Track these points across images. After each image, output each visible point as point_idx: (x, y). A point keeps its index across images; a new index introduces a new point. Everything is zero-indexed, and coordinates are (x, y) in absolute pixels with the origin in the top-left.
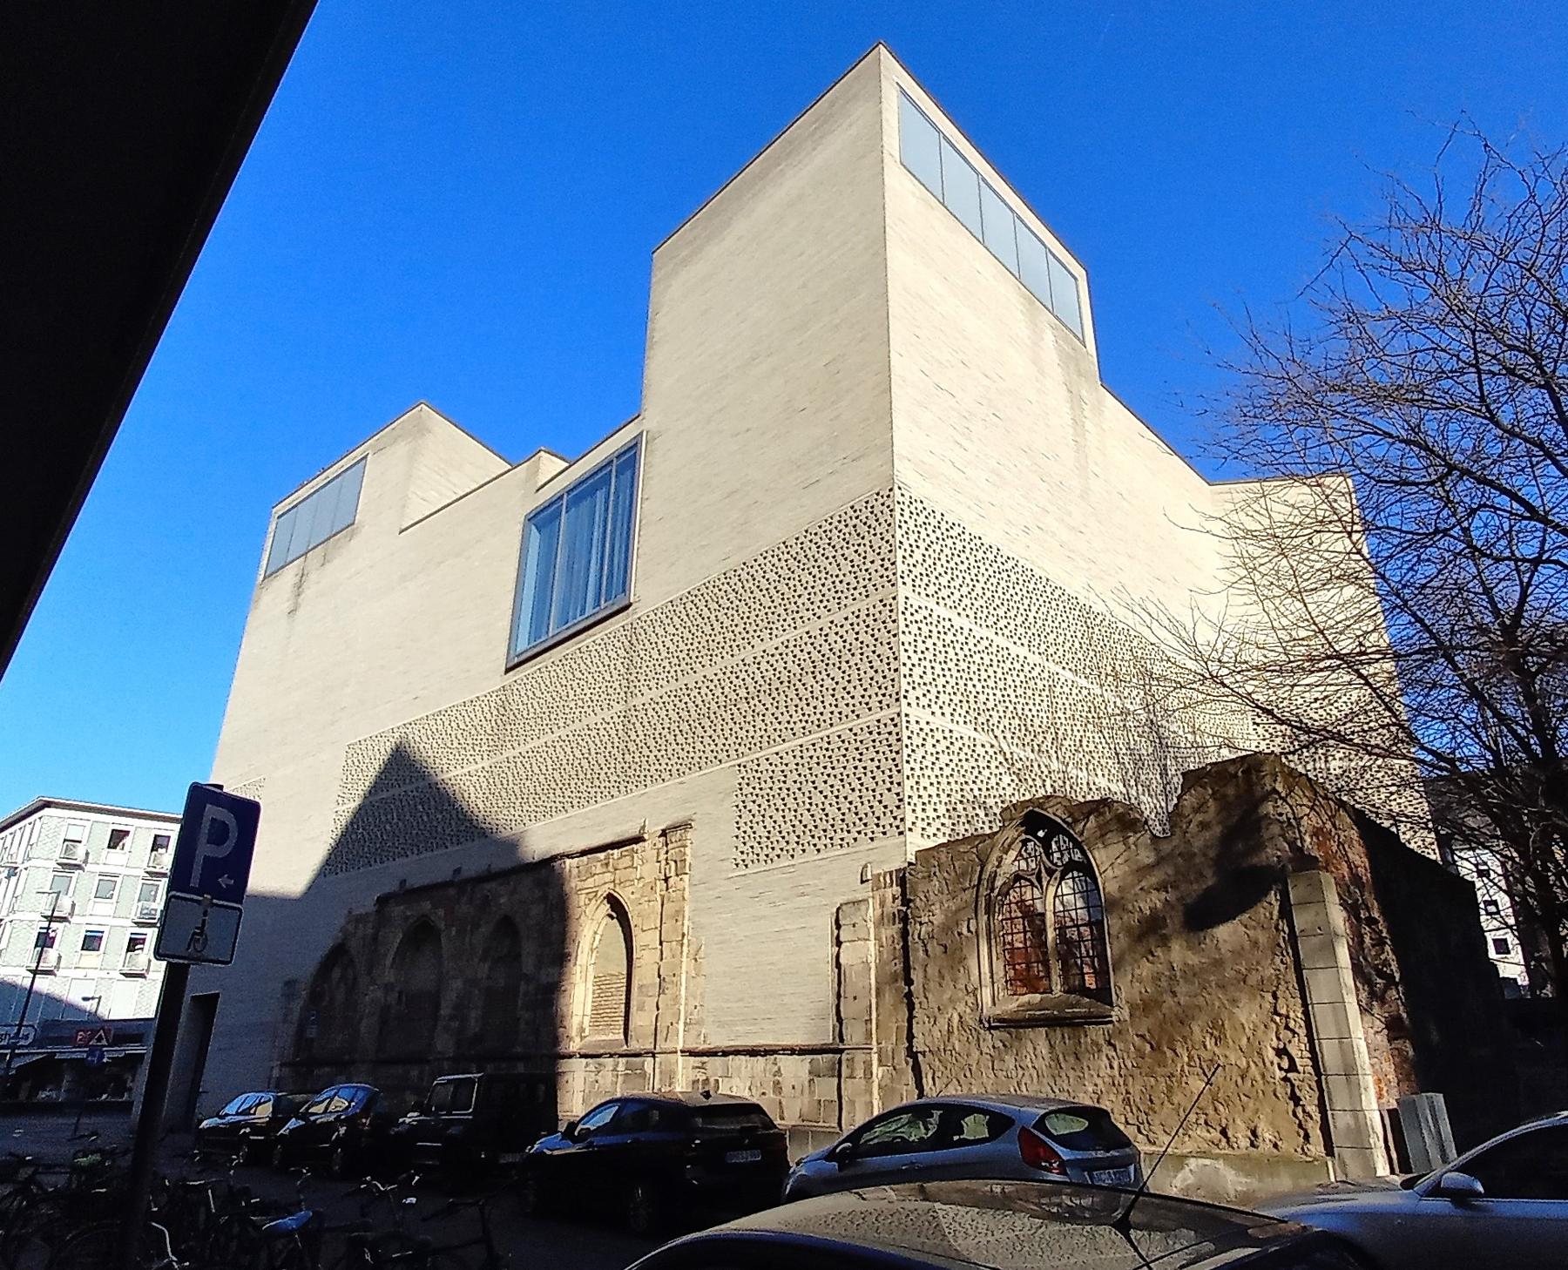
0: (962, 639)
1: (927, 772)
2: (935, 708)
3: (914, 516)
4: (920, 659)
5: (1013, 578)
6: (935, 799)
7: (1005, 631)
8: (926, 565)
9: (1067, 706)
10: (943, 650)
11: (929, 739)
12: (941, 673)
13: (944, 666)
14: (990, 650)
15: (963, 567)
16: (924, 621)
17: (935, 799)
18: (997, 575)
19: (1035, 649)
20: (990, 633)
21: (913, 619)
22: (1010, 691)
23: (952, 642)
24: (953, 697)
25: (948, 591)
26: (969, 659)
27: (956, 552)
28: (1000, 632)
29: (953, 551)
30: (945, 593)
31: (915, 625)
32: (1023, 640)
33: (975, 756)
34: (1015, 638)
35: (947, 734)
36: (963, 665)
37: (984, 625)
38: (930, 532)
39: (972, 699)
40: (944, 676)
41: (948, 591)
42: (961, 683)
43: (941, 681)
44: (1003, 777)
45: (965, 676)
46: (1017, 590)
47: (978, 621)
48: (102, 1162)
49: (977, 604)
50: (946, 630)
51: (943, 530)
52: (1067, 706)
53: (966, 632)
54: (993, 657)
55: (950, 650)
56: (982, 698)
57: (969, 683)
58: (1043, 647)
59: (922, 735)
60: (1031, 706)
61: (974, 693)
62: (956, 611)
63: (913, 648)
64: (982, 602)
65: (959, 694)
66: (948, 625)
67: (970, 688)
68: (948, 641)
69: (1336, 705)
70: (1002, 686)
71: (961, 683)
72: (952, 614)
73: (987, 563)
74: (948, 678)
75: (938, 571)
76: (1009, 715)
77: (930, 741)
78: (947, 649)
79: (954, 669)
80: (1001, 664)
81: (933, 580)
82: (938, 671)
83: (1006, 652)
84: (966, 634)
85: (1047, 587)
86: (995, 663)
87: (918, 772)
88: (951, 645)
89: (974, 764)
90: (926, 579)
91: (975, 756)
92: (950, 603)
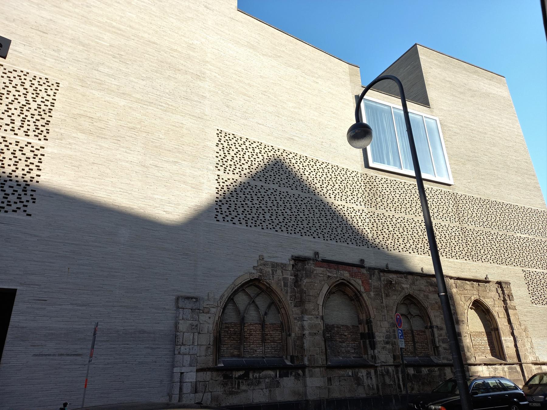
0: (495, 237)
1: (539, 286)
2: (537, 267)
3: (447, 197)
4: (340, 224)
5: (510, 211)
6: (543, 293)
7: (487, 226)
8: (501, 221)
9: (519, 246)
10: (489, 242)
11: (537, 276)
12: (466, 246)
13: (536, 253)
14: (483, 233)
15: (442, 204)
16: (371, 217)
17: (543, 293)
18: (526, 216)
19: (523, 233)
20: (527, 236)
21: (501, 239)
22: (538, 252)
23: (355, 216)
24: (496, 256)
25: (510, 227)
26: (543, 249)
27: (439, 200)
28: (509, 231)
29: (438, 199)
30: (509, 227)
31: (479, 237)
32: (496, 227)
33: (531, 276)
34: (469, 223)
35: (542, 274)
36: (542, 251)
37: (502, 230)
38: (500, 210)
39: (503, 255)
40: (382, 234)
41: (510, 227)
42: (521, 254)
43: (536, 258)
44: (542, 280)
45: (499, 248)
46: (533, 218)
47: (543, 236)
48: (528, 404)
49: (498, 224)
50: (382, 218)
51: (504, 207)
52: (519, 246)
53: (540, 241)
54: (530, 243)
55: (492, 241)
56: (529, 257)
57: (524, 253)
58: (481, 223)
59: (535, 275)
60: (526, 253)
61: (503, 253)
62: (467, 224)
63: (367, 227)
64: (500, 222)
65: (498, 255)
66: (489, 234)
67: (477, 248)
68: (353, 216)
69: (9, 75)
70: (466, 242)
71: (521, 254)
72: (354, 205)
73: (541, 217)
74: (538, 257)
75: (399, 203)
76: (539, 260)
77: (537, 277)
78: (491, 241)
79: (539, 253)
80: (533, 244)
81: (526, 228)
82: (513, 252)
83: (512, 237)
84: (519, 238)
85: (504, 205)
86: (534, 215)
87: (536, 287)
88: (355, 217)
89: (531, 278)
90: (524, 229)
91: (531, 276)
92: (532, 233)
